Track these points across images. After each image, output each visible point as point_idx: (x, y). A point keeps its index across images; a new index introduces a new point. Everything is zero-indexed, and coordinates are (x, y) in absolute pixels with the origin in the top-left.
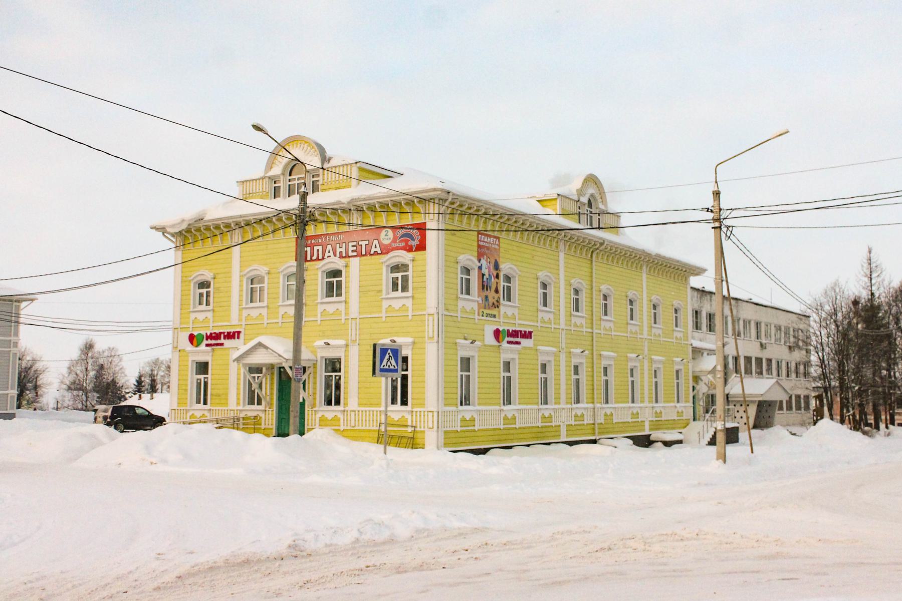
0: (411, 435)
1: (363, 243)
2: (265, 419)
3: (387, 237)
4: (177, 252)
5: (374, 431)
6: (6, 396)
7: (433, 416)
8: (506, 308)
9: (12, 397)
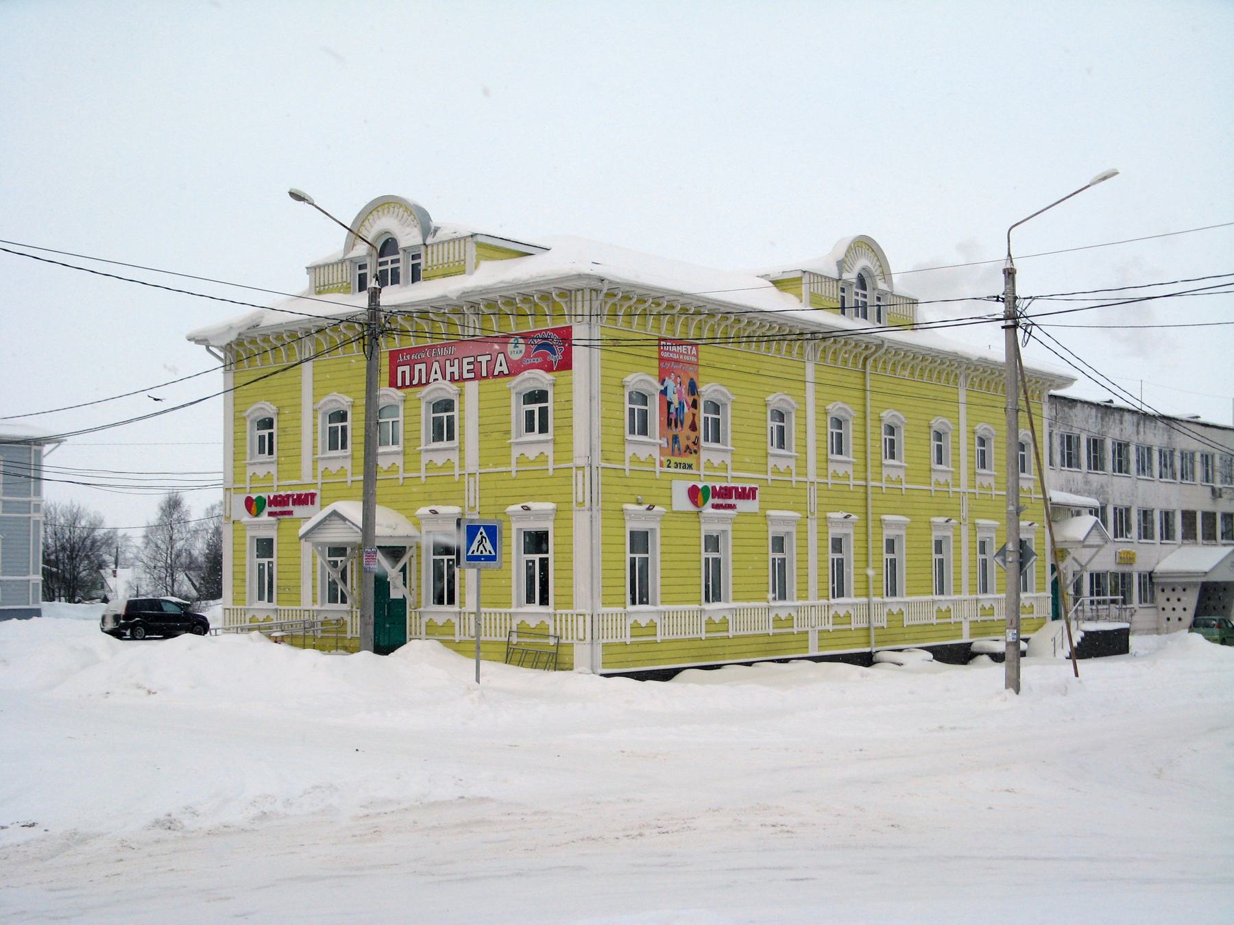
0: (554, 650)
1: (484, 359)
2: (352, 624)
3: (516, 352)
4: (227, 374)
5: (500, 643)
6: (27, 583)
7: (584, 621)
8: (710, 453)
9: (36, 585)
